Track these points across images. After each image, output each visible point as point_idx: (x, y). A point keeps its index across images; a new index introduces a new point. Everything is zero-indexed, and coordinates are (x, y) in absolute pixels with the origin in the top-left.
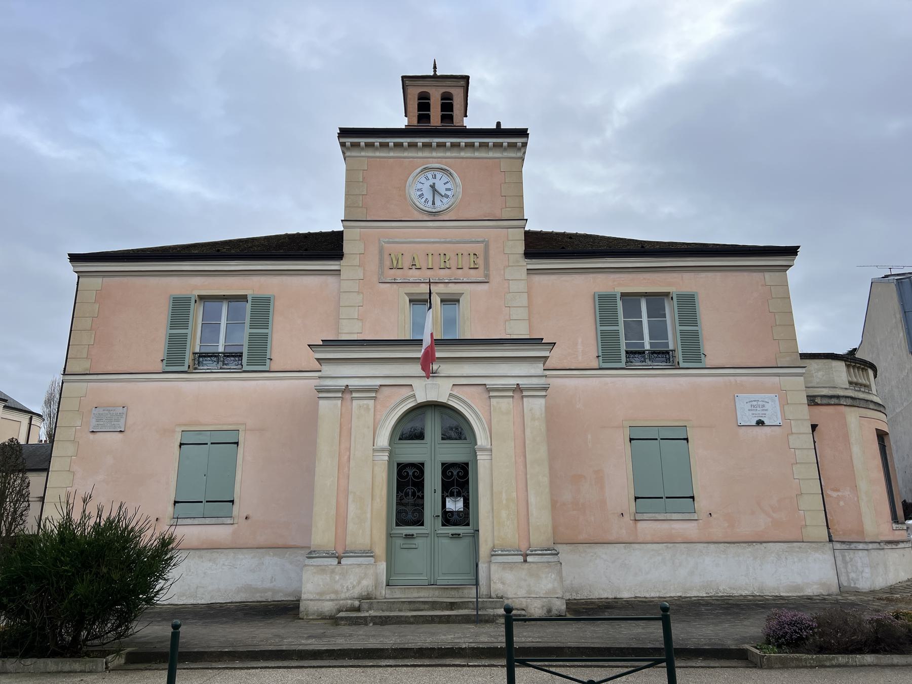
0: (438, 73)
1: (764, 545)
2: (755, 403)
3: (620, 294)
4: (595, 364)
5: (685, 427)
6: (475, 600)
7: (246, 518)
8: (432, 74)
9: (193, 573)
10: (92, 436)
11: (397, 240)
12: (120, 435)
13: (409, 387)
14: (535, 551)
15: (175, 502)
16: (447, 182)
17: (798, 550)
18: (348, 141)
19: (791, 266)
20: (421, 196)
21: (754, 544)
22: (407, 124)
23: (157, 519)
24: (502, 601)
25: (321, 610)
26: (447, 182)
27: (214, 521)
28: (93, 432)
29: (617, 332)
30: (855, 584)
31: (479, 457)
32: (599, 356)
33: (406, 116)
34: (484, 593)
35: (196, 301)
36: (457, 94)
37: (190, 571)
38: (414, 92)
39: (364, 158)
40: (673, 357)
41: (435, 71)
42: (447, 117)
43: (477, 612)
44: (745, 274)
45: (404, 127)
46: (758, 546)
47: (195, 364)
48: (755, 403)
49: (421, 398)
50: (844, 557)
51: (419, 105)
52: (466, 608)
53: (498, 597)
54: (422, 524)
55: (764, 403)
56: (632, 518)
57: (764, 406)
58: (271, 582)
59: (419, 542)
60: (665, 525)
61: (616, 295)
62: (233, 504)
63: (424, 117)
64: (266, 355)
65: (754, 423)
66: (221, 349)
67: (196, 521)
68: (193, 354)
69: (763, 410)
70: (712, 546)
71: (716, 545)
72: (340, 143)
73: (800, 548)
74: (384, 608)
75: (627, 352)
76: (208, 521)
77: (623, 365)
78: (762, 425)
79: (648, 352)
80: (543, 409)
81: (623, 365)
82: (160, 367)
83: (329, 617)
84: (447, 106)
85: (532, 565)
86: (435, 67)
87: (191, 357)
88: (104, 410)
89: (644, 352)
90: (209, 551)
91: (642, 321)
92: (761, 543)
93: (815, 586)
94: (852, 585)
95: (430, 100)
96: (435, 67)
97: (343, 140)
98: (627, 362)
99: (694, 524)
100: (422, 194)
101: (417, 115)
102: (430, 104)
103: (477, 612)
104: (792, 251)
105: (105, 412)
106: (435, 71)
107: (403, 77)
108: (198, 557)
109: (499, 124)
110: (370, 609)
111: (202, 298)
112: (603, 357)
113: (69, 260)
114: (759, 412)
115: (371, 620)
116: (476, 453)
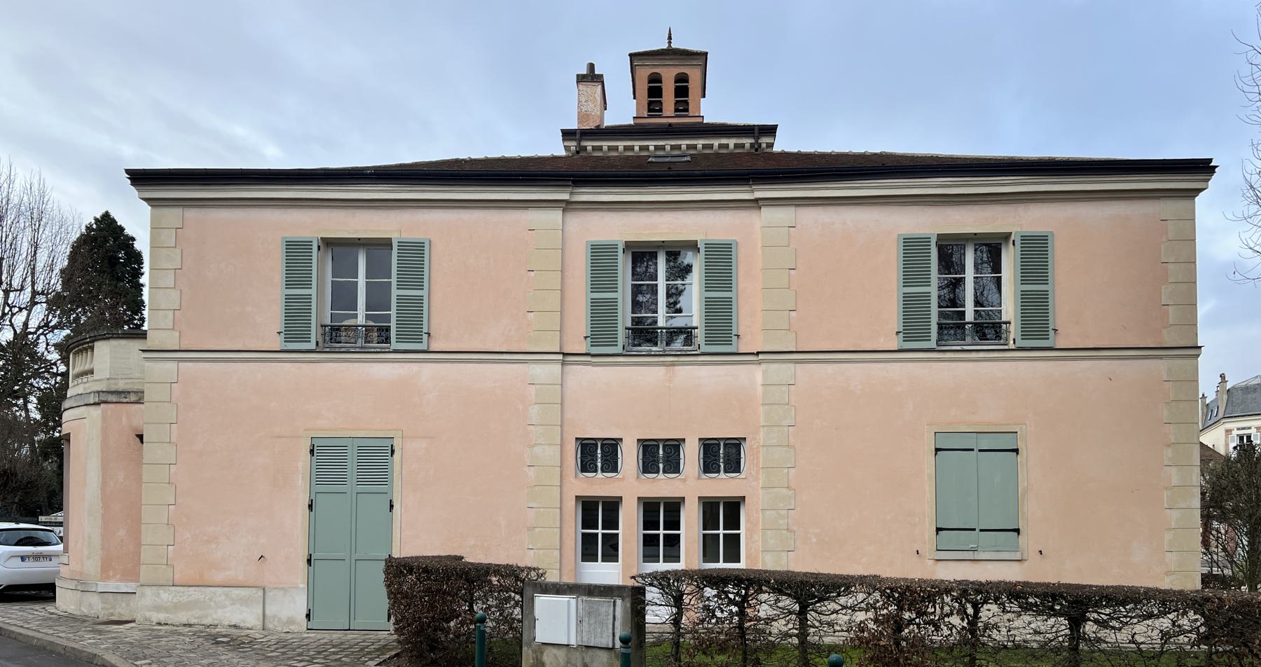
0: (674, 46)
8: (665, 46)
19: (1205, 189)
22: (635, 116)
24: (664, 446)
29: (928, 294)
32: (900, 332)
33: (635, 98)
35: (319, 247)
36: (694, 74)
38: (644, 73)
41: (670, 43)
42: (682, 106)
45: (632, 122)
47: (325, 340)
51: (650, 89)
62: (1019, 534)
63: (654, 106)
64: (422, 328)
68: (322, 326)
72: (564, 146)
75: (941, 327)
77: (932, 344)
80: (630, 610)
81: (932, 344)
82: (278, 343)
84: (682, 92)
86: (670, 38)
87: (320, 330)
95: (661, 83)
96: (670, 38)
97: (567, 144)
101: (646, 88)
102: (662, 89)
104: (1203, 168)
106: (670, 43)
107: (631, 55)
113: (129, 181)
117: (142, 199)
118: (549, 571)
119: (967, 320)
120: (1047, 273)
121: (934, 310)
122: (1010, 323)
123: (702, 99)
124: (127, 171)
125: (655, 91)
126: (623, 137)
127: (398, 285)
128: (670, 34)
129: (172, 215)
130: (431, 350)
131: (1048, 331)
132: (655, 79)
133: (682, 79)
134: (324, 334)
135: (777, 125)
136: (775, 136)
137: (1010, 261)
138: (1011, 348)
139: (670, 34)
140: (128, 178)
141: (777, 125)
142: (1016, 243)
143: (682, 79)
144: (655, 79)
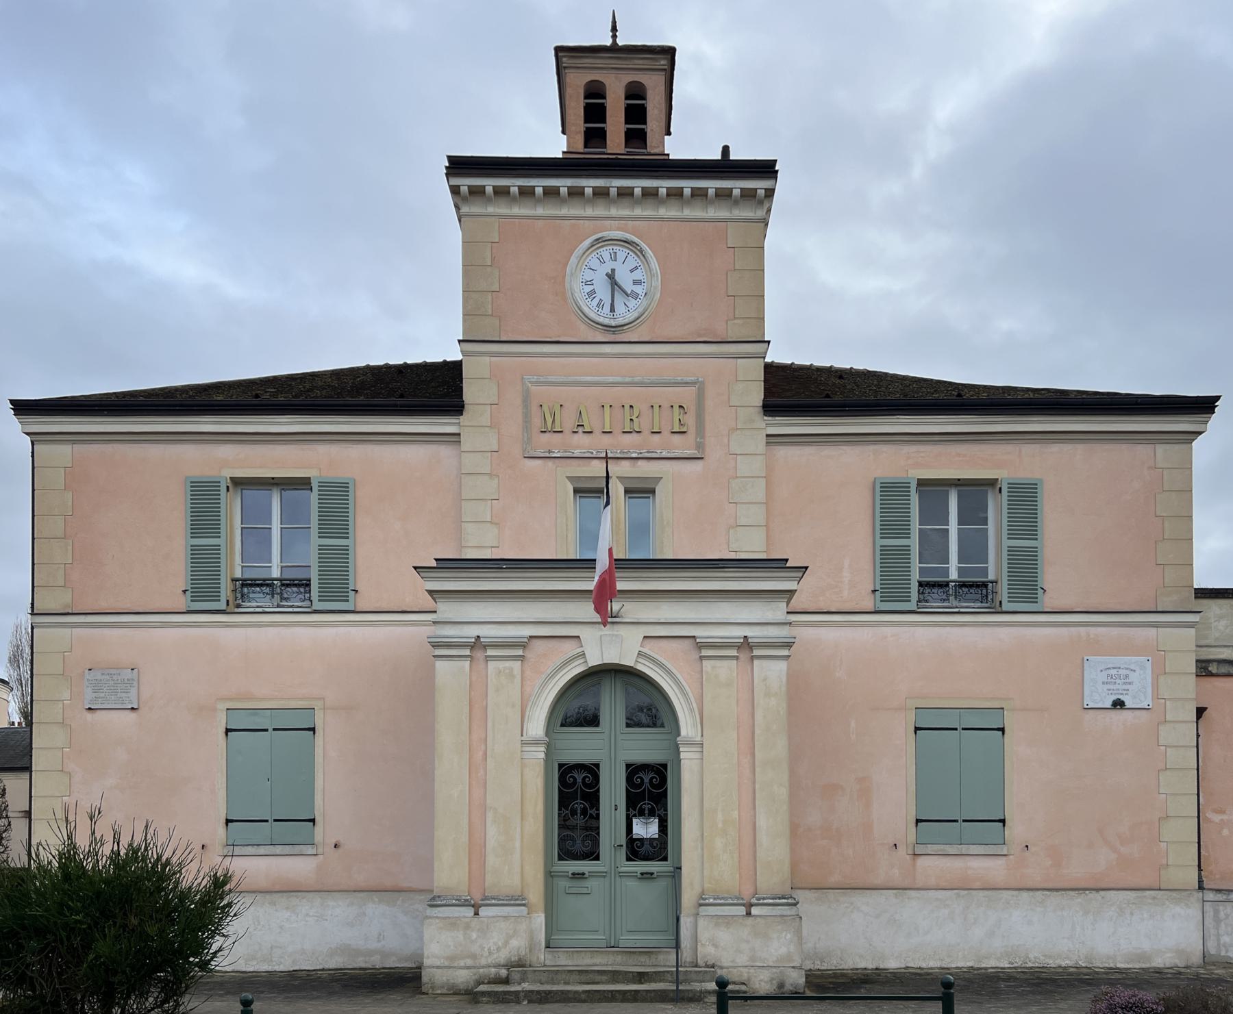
1: (1102, 893)
2: (1113, 672)
4: (868, 604)
6: (675, 969)
9: (263, 926)
10: (89, 715)
11: (552, 378)
12: (133, 715)
13: (576, 639)
14: (764, 899)
16: (636, 268)
17: (1150, 901)
18: (465, 182)
19: (1204, 432)
20: (592, 294)
21: (1087, 892)
23: (203, 846)
26: (636, 268)
27: (287, 849)
28: (90, 709)
29: (907, 548)
30: (1227, 952)
31: (682, 755)
32: (876, 591)
33: (564, 132)
34: (688, 960)
36: (653, 83)
37: (259, 923)
38: (578, 81)
39: (493, 219)
41: (614, 37)
42: (636, 137)
43: (677, 987)
44: (1124, 447)
45: (560, 156)
46: (1093, 895)
48: (1113, 672)
49: (594, 660)
50: (1216, 912)
52: (661, 981)
53: (707, 966)
57: (1127, 676)
58: (379, 941)
59: (591, 884)
60: (958, 863)
63: (595, 136)
65: (1109, 705)
66: (276, 573)
67: (262, 850)
68: (233, 580)
70: (1025, 894)
71: (1031, 893)
72: (451, 187)
73: (1154, 898)
74: (543, 980)
75: (921, 584)
76: (278, 850)
77: (912, 605)
78: (1121, 708)
81: (912, 605)
82: (182, 602)
84: (636, 114)
85: (759, 920)
86: (614, 29)
87: (230, 586)
88: (103, 674)
90: (285, 894)
92: (1097, 890)
93: (1169, 955)
94: (1223, 953)
96: (614, 29)
97: (456, 181)
98: (919, 601)
99: (1000, 862)
100: (594, 292)
101: (582, 129)
103: (677, 987)
105: (104, 677)
106: (614, 37)
107: (558, 50)
108: (269, 903)
109: (726, 150)
110: (523, 980)
111: (238, 483)
112: (881, 593)
113: (12, 412)
115: (525, 997)
116: (678, 749)
117: (25, 433)
118: (13, 841)
119: (951, 578)
120: (1036, 526)
121: (915, 565)
122: (996, 582)
123: (666, 137)
124: (12, 402)
125: (595, 112)
126: (538, 172)
127: (319, 533)
128: (614, 22)
129: (62, 453)
130: (357, 610)
131: (1037, 590)
132: (595, 92)
133: (635, 93)
134: (235, 591)
135: (776, 161)
136: (776, 178)
137: (996, 510)
138: (998, 611)
139: (614, 22)
140: (11, 408)
141: (776, 161)
142: (1003, 489)
143: (635, 93)
144: (595, 92)
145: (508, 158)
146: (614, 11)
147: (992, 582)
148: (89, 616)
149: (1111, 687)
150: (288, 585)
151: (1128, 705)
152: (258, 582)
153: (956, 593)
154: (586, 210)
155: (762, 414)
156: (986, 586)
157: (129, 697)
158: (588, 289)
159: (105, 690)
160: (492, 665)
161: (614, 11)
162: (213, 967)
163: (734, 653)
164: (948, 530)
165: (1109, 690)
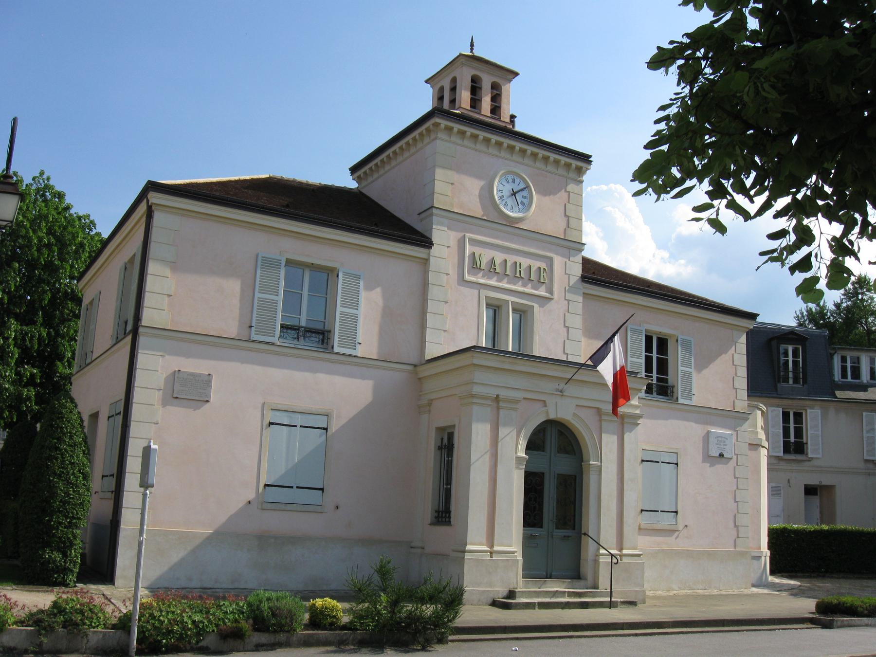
2: (720, 439)
3: (285, 261)
5: (675, 455)
7: (337, 507)
15: (103, 476)
23: (337, 508)
25: (827, 601)
28: (177, 398)
29: (276, 302)
40: (328, 338)
48: (720, 439)
54: (541, 527)
55: (725, 440)
56: (260, 507)
57: (724, 442)
61: (281, 261)
65: (717, 455)
66: (303, 323)
69: (724, 445)
75: (282, 326)
79: (303, 329)
83: (80, 611)
86: (472, 45)
89: (299, 327)
91: (652, 356)
96: (472, 45)
98: (280, 336)
109: (830, 223)
111: (289, 262)
112: (256, 328)
114: (721, 447)
145: (567, 148)
146: (472, 37)
147: (327, 332)
148: (178, 333)
149: (718, 446)
150: (308, 331)
151: (725, 456)
152: (295, 327)
153: (304, 335)
154: (513, 156)
155: (581, 281)
156: (298, 330)
157: (205, 393)
158: (501, 194)
159: (189, 386)
160: (475, 408)
161: (472, 37)
162: (371, 593)
163: (489, 402)
164: (309, 292)
165: (718, 448)
